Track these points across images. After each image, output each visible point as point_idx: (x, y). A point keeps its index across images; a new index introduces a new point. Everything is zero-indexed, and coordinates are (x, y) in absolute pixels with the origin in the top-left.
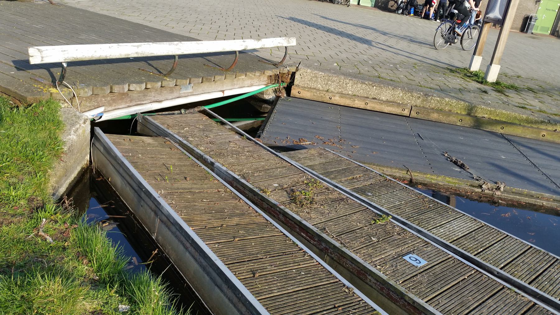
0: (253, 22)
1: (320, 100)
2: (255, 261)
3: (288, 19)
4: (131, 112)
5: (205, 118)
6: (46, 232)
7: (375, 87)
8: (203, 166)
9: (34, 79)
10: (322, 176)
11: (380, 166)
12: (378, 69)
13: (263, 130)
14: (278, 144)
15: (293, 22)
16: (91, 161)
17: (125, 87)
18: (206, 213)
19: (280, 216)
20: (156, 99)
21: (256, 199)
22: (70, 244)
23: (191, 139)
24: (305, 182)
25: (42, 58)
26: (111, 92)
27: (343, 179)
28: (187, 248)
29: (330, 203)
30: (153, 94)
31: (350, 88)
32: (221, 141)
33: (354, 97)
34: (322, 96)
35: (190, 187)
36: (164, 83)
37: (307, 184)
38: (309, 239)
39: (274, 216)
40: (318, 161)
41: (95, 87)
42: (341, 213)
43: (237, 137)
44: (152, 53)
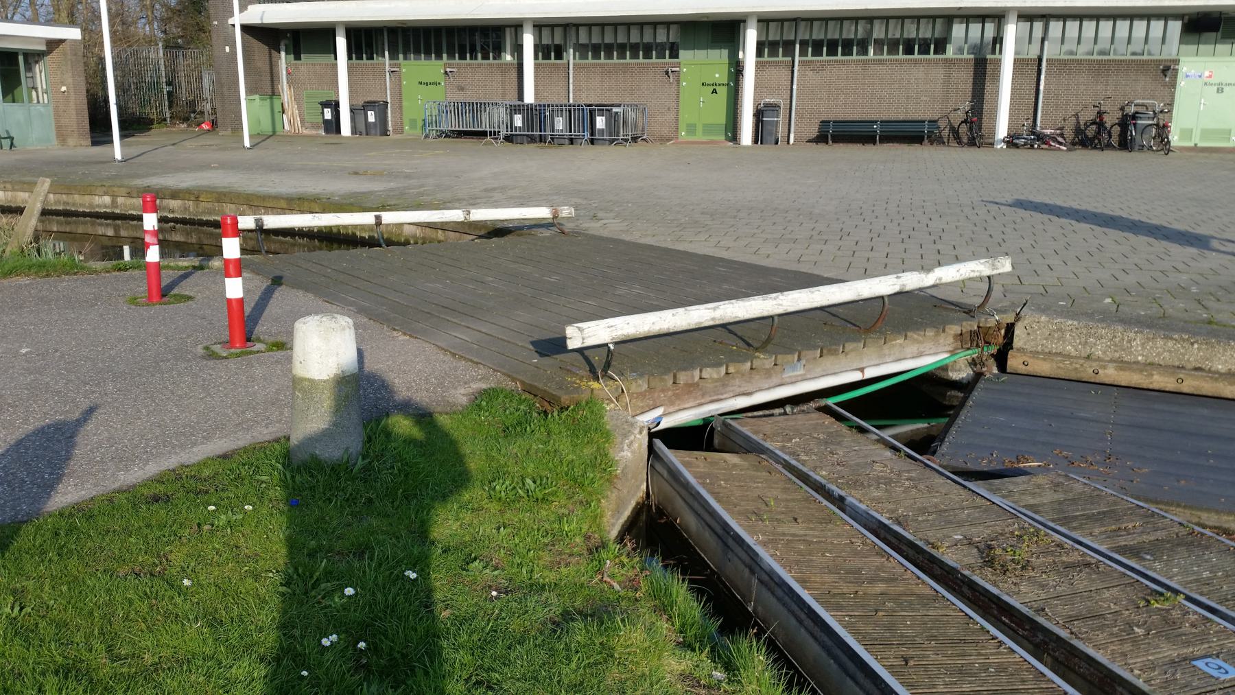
0: (929, 222)
1: (1073, 376)
2: (911, 646)
3: (1010, 206)
4: (701, 414)
5: (828, 420)
6: (612, 577)
7: (1196, 346)
8: (825, 502)
9: (565, 369)
10: (1052, 524)
11: (1191, 508)
12: (1212, 304)
13: (942, 441)
14: (971, 466)
15: (1021, 212)
16: (648, 493)
17: (695, 374)
18: (830, 572)
19: (963, 589)
20: (742, 390)
21: (921, 559)
22: (642, 595)
23: (803, 458)
24: (1016, 533)
25: (583, 339)
26: (674, 383)
27: (1097, 531)
28: (800, 622)
29: (1062, 570)
30: (737, 382)
31: (1140, 348)
32: (858, 461)
33: (1149, 368)
34: (1076, 369)
35: (802, 532)
36: (756, 363)
37: (1020, 537)
38: (1016, 628)
39: (954, 590)
40: (1048, 497)
41: (651, 378)
42: (1081, 586)
43: (888, 453)
44: (736, 317)
